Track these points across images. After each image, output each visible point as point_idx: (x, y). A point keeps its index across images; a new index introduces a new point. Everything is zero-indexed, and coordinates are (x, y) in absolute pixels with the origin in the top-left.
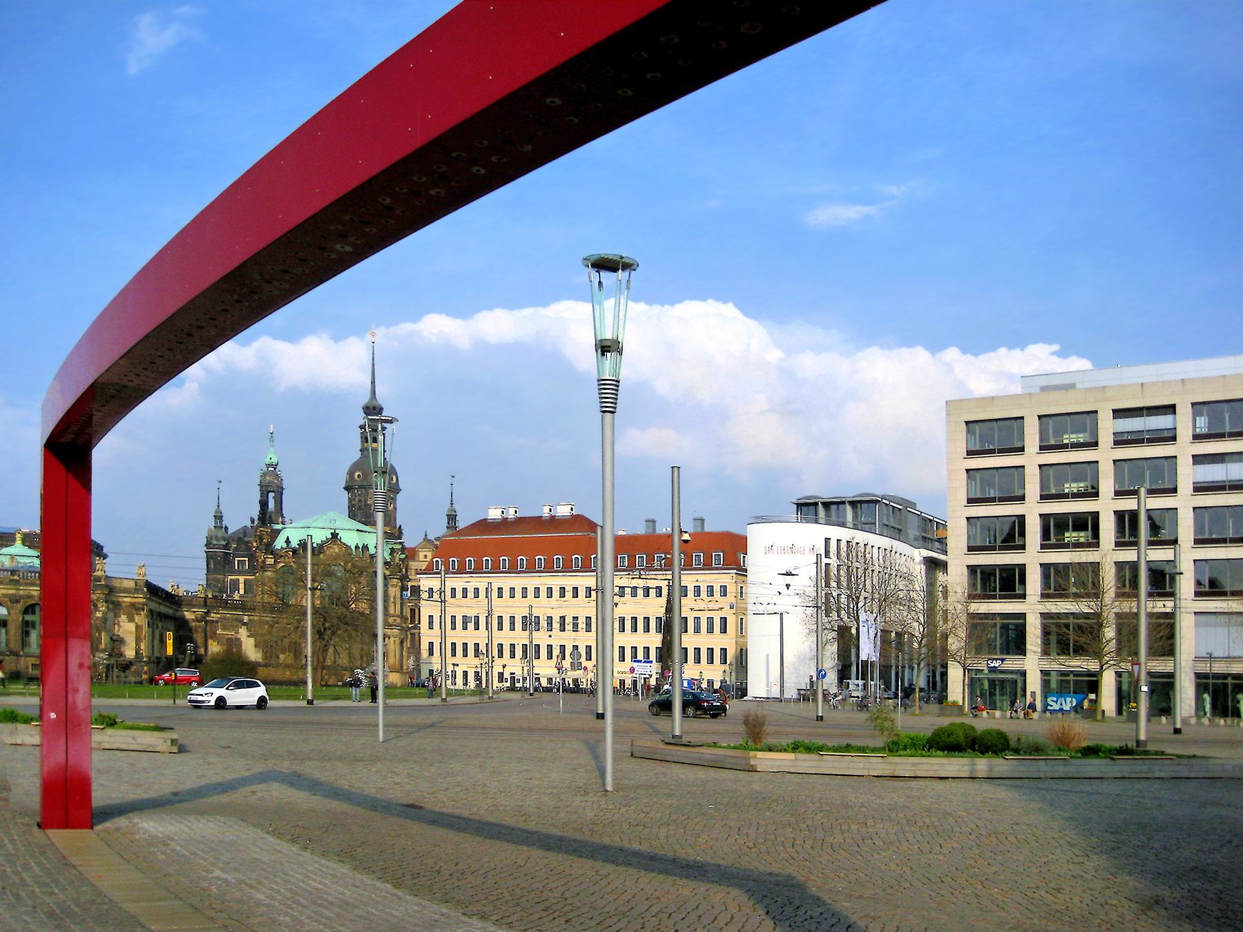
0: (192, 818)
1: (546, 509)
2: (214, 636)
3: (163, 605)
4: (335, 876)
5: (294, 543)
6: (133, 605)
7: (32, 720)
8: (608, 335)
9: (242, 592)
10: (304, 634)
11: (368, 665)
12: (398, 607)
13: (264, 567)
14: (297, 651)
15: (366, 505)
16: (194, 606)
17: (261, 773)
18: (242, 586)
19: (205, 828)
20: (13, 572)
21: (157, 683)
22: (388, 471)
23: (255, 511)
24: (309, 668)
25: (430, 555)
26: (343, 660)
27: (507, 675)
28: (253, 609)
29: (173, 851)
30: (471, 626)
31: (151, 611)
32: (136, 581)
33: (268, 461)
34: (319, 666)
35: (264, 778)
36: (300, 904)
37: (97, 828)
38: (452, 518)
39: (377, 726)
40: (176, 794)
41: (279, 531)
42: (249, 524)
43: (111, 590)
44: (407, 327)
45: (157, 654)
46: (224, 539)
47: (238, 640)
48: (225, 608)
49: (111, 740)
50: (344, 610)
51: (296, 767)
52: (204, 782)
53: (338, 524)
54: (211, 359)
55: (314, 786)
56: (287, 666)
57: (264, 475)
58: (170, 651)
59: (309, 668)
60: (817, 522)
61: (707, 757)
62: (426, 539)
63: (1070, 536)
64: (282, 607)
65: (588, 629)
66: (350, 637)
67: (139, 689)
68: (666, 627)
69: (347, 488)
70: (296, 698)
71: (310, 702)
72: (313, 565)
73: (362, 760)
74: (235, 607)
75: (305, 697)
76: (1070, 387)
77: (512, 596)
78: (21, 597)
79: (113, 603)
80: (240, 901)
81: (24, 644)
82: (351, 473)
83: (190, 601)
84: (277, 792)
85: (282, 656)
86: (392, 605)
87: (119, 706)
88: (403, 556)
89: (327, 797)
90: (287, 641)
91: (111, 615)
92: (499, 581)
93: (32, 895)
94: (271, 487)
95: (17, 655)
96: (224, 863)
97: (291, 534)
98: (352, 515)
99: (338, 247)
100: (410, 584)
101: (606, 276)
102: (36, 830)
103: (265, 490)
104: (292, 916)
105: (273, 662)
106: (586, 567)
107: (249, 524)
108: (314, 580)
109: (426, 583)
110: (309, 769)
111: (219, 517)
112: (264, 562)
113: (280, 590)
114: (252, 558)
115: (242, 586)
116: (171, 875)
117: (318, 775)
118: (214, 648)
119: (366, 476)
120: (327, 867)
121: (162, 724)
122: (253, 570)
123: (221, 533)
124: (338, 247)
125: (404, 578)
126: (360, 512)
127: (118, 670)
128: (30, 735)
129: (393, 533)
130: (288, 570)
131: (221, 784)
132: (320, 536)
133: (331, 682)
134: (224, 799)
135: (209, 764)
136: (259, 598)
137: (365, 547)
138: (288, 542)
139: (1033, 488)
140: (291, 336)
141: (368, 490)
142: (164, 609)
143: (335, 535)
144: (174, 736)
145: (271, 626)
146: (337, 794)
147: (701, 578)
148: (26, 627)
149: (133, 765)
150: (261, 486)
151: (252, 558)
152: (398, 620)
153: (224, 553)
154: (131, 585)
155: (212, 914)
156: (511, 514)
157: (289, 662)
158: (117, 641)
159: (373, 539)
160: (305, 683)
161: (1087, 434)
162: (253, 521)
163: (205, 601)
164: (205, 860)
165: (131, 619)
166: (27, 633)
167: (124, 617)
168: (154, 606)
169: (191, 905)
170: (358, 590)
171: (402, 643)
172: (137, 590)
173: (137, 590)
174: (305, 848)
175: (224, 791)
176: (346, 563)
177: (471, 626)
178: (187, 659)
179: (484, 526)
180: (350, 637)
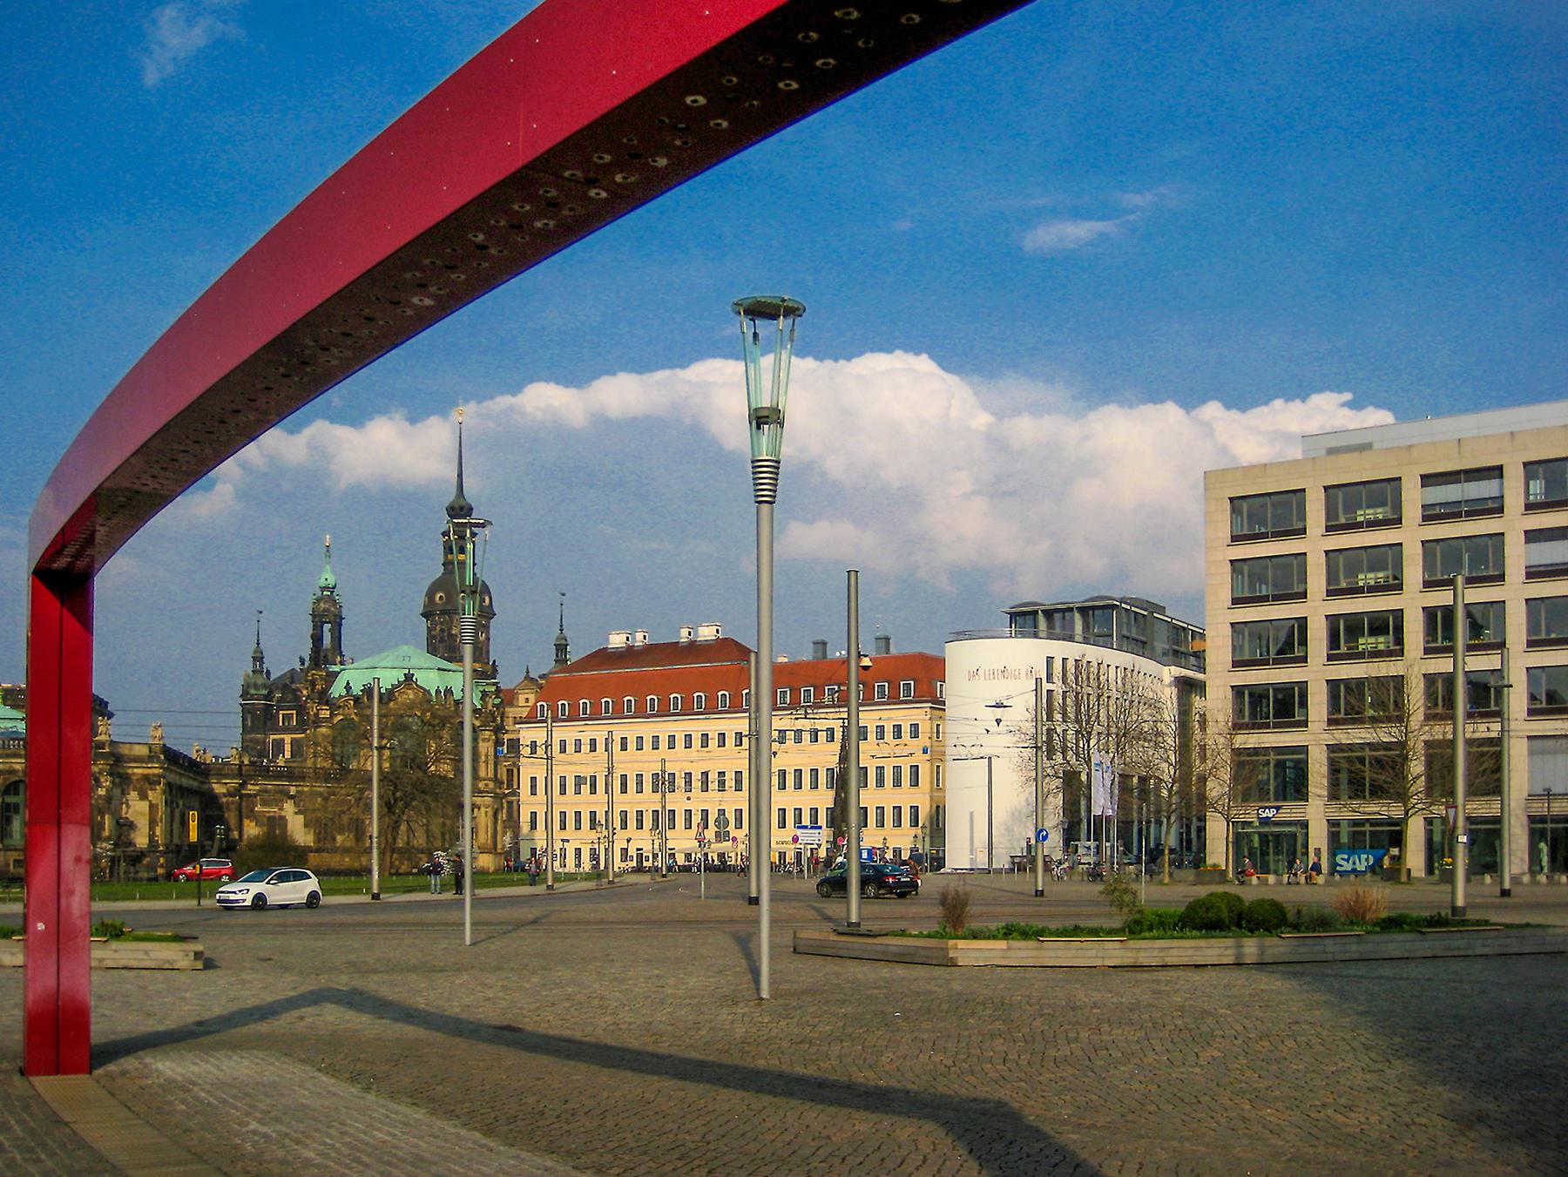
1: (684, 632)
3: (186, 779)
5: (357, 690)
6: (146, 778)
9: (288, 755)
10: (368, 807)
11: (452, 845)
13: (317, 722)
14: (359, 831)
15: (451, 635)
17: (312, 992)
18: (288, 748)
19: (237, 1067)
21: (177, 880)
23: (306, 653)
24: (375, 852)
25: (532, 698)
26: (420, 840)
27: (632, 852)
28: (302, 778)
29: (196, 1098)
30: (586, 788)
31: (169, 785)
33: (322, 583)
34: (388, 848)
37: (96, 1072)
40: (200, 1023)
41: (336, 674)
42: (298, 666)
45: (176, 841)
46: (265, 686)
47: (283, 818)
48: (265, 777)
49: (116, 956)
50: (420, 774)
51: (358, 982)
52: (236, 1006)
53: (414, 662)
55: (379, 1006)
56: (346, 851)
57: (319, 600)
58: (193, 836)
59: (375, 852)
60: (1036, 636)
61: (892, 949)
63: (1366, 578)
64: (341, 773)
66: (428, 809)
67: (155, 887)
70: (358, 891)
71: (376, 897)
72: (381, 716)
73: (442, 970)
74: (279, 775)
75: (369, 890)
76: (1367, 447)
79: (120, 776)
80: (283, 1162)
82: (430, 594)
83: (221, 771)
84: (332, 1016)
85: (339, 838)
87: (128, 912)
90: (345, 818)
91: (117, 791)
94: (327, 615)
96: (262, 1112)
97: (352, 677)
98: (432, 650)
99: (415, 300)
100: (506, 737)
102: (17, 1078)
103: (318, 619)
107: (298, 666)
108: (381, 737)
109: (527, 735)
110: (374, 984)
111: (258, 658)
112: (316, 715)
114: (301, 710)
115: (288, 748)
116: (192, 1131)
117: (386, 992)
118: (252, 830)
119: (450, 597)
121: (184, 932)
122: (302, 725)
123: (260, 680)
124: (415, 300)
125: (499, 730)
130: (347, 720)
131: (258, 1008)
133: (404, 868)
134: (264, 1027)
135: (244, 982)
136: (309, 763)
137: (449, 691)
138: (348, 687)
139: (1317, 581)
140: (356, 418)
142: (185, 782)
144: (199, 947)
145: (326, 799)
146: (408, 1015)
147: (885, 715)
151: (301, 710)
152: (491, 785)
153: (268, 703)
154: (144, 751)
156: (639, 640)
157: (348, 844)
159: (458, 680)
160: (370, 871)
161: (1388, 509)
162: (302, 661)
163: (240, 769)
164: (237, 1108)
165: (143, 796)
167: (134, 794)
170: (439, 748)
172: (150, 759)
174: (368, 1089)
175: (263, 1018)
176: (423, 713)
177: (586, 788)
178: (216, 845)
179: (604, 657)
180: (428, 809)
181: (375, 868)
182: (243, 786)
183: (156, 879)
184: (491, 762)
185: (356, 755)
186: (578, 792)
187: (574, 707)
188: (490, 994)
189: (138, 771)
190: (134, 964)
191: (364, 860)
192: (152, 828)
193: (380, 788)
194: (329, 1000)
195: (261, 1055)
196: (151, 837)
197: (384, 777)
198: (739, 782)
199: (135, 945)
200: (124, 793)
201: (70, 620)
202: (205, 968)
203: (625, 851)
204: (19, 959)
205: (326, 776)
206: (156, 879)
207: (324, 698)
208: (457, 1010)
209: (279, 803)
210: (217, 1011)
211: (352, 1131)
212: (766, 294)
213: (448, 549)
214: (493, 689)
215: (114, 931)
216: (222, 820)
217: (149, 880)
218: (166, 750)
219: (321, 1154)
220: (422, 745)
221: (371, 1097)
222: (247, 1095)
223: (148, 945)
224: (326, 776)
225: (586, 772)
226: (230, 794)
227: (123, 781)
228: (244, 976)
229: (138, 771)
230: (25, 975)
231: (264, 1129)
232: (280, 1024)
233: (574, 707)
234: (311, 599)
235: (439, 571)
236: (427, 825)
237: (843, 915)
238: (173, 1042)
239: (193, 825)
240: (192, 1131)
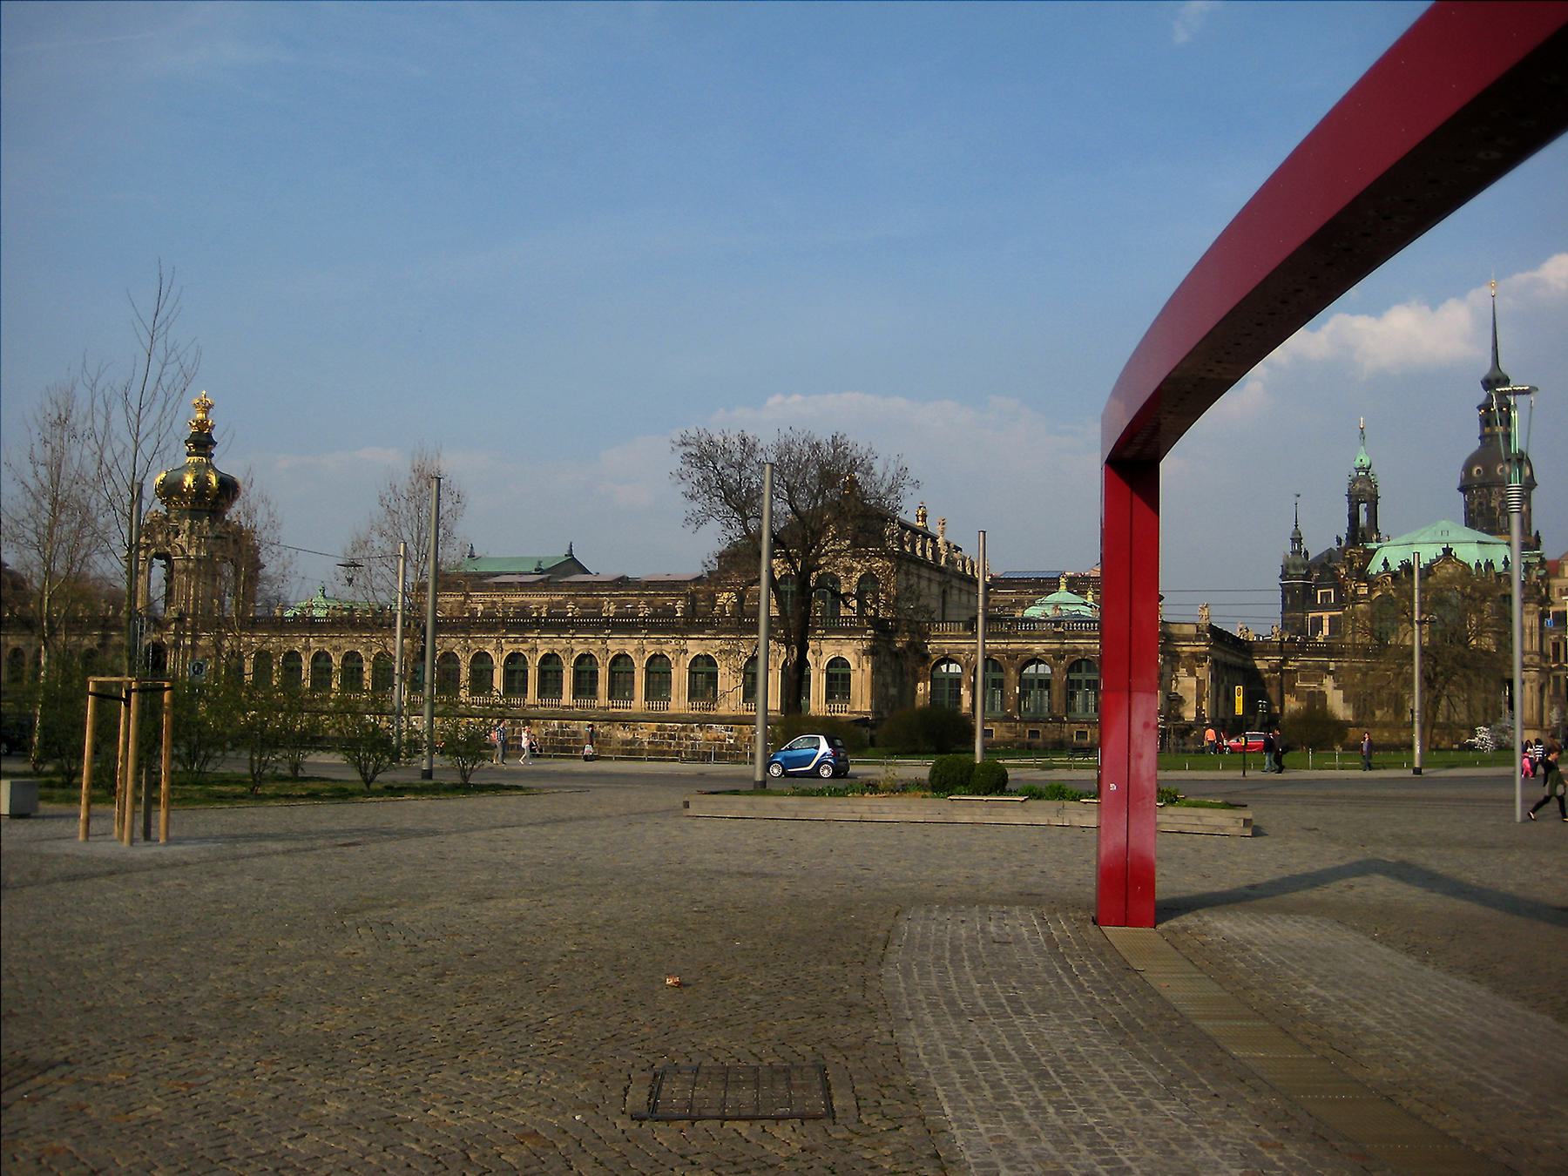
0: (1274, 917)
2: (1292, 690)
3: (1230, 654)
4: (1468, 1001)
5: (1395, 566)
6: (1193, 655)
7: (1081, 796)
9: (1326, 631)
10: (1409, 682)
11: (1495, 720)
13: (1356, 599)
14: (1399, 706)
17: (1359, 863)
18: (1326, 623)
19: (1293, 931)
20: (1058, 623)
21: (1222, 752)
23: (1343, 533)
24: (1417, 726)
26: (1461, 716)
28: (1341, 653)
29: (1255, 957)
31: (1215, 662)
33: (1357, 464)
34: (1429, 723)
35: (1365, 868)
36: (1423, 1035)
37: (1159, 927)
39: (1513, 801)
40: (1253, 887)
41: (1374, 551)
42: (1335, 546)
43: (1169, 638)
44: (1521, 278)
45: (1221, 715)
48: (1305, 654)
49: (1171, 820)
50: (1461, 649)
51: (1403, 855)
52: (1286, 873)
53: (1453, 536)
54: (1277, 354)
55: (1430, 880)
56: (1385, 726)
57: (1354, 481)
58: (1239, 710)
59: (1417, 726)
64: (1380, 647)
66: (1470, 683)
67: (1201, 758)
69: (1462, 489)
70: (1400, 766)
72: (1421, 591)
73: (1493, 846)
74: (1318, 652)
75: (1410, 764)
78: (1066, 651)
79: (1170, 653)
80: (1343, 1026)
81: (1069, 707)
82: (1468, 468)
83: (1263, 648)
84: (1380, 887)
85: (1378, 713)
86: (1527, 637)
87: (1180, 781)
88: (1542, 572)
89: (1448, 894)
90: (1384, 694)
91: (1167, 669)
93: (1091, 1003)
94: (1363, 495)
95: (1060, 720)
96: (1321, 976)
97: (1389, 554)
98: (1471, 522)
99: (1481, 155)
100: (1552, 610)
102: (1090, 926)
103: (1354, 500)
104: (1413, 1050)
105: (1367, 720)
107: (1335, 546)
108: (1421, 612)
110: (1421, 857)
111: (1297, 539)
112: (1355, 591)
113: (1376, 626)
114: (1340, 588)
115: (1326, 623)
116: (1253, 989)
117: (1434, 866)
118: (1292, 704)
119: (1488, 469)
120: (1457, 988)
121: (1233, 800)
122: (1340, 603)
123: (1300, 560)
124: (1481, 155)
125: (1545, 601)
126: (1484, 515)
127: (1177, 737)
128: (1084, 816)
129: (1531, 542)
130: (1386, 598)
131: (1306, 876)
132: (1429, 553)
133: (1444, 744)
134: (1315, 894)
135: (1291, 850)
136: (1348, 639)
137: (1490, 565)
138: (1386, 564)
140: (1376, 309)
142: (1231, 659)
143: (1447, 551)
144: (1248, 815)
145: (1365, 674)
146: (1458, 889)
148: (1071, 687)
149: (1199, 851)
150: (1350, 496)
151: (1340, 588)
152: (1537, 659)
153: (1307, 580)
154: (1192, 630)
155: (1307, 1040)
157: (1387, 719)
158: (1175, 701)
159: (1498, 553)
160: (1411, 747)
162: (1339, 541)
163: (1281, 646)
164: (1293, 970)
165: (1192, 673)
166: (1073, 696)
168: (1219, 655)
169: (1281, 1028)
170: (1481, 622)
171: (1541, 689)
172: (1198, 637)
173: (1199, 636)
174: (1425, 962)
175: (1313, 885)
176: (1464, 588)
178: (1258, 720)
180: (1470, 683)
181: (1417, 743)
182: (1284, 662)
183: (1202, 751)
185: (1395, 631)
188: (1547, 873)
189: (1186, 649)
190: (1187, 829)
191: (1404, 735)
192: (1199, 703)
193: (1421, 661)
194: (1377, 871)
195: (1314, 920)
196: (1199, 711)
197: (1424, 652)
199: (1188, 811)
200: (1174, 670)
201: (1140, 505)
202: (1254, 835)
204: (1092, 820)
205: (1365, 652)
206: (1202, 751)
207: (1362, 575)
208: (1511, 888)
210: (1268, 877)
211: (1412, 1002)
213: (1486, 421)
214: (1537, 560)
215: (1170, 798)
216: (1264, 696)
217: (1197, 751)
218: (1213, 629)
219: (1381, 1022)
220: (1463, 619)
221: (1428, 970)
222: (1304, 958)
223: (1201, 811)
224: (1365, 652)
226: (1272, 670)
227: (1174, 658)
228: (1291, 844)
229: (1186, 649)
230: (1099, 835)
231: (1322, 993)
232: (1330, 892)
234: (1348, 480)
235: (1476, 444)
236: (1468, 700)
238: (1229, 902)
239: (1239, 700)
240: (1253, 989)
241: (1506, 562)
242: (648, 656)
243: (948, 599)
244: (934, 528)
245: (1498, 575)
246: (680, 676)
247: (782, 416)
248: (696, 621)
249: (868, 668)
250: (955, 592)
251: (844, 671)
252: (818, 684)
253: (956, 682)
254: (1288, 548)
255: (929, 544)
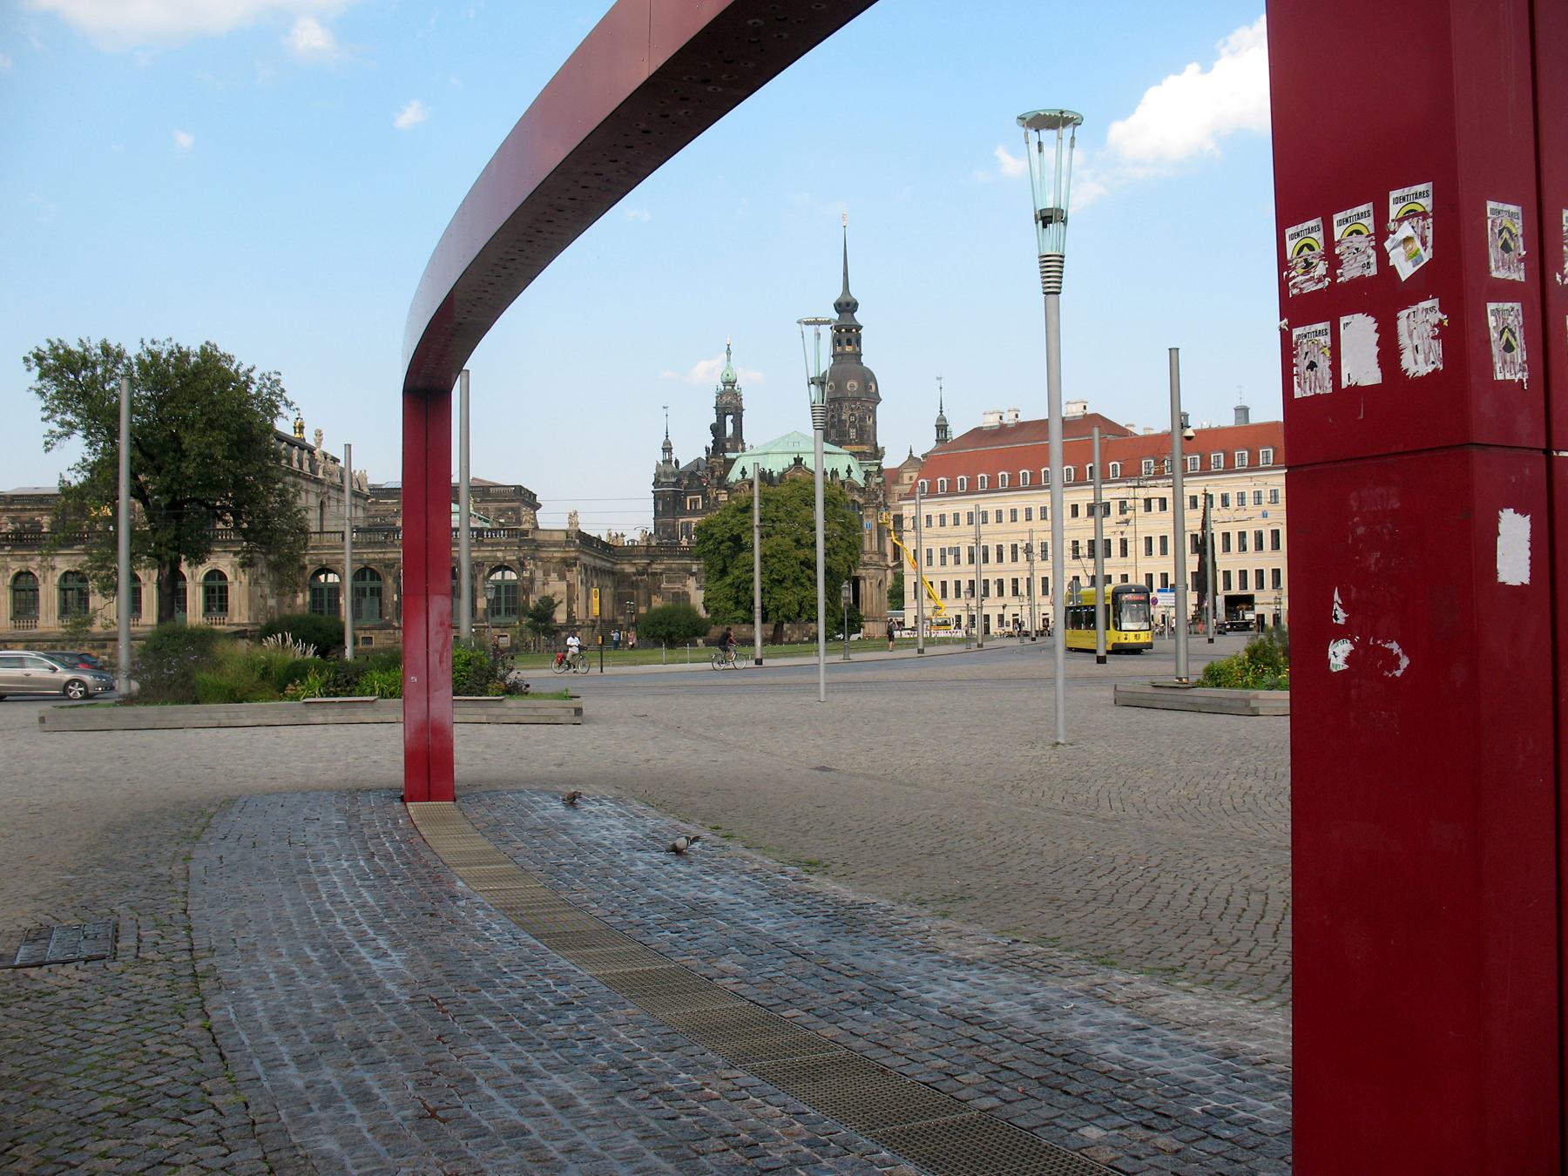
2: (658, 590)
8: (1049, 203)
12: (875, 542)
15: (840, 421)
16: (635, 556)
22: (867, 379)
23: (708, 440)
25: (915, 475)
27: (1008, 618)
32: (567, 532)
38: (942, 427)
41: (733, 461)
46: (673, 474)
47: (686, 594)
57: (720, 395)
61: (1200, 700)
62: (911, 456)
65: (1164, 551)
68: (1201, 545)
71: (759, 662)
74: (683, 555)
77: (1014, 520)
83: (629, 552)
92: (990, 504)
94: (729, 406)
101: (1048, 135)
102: (397, 804)
103: (721, 412)
106: (1036, 484)
109: (908, 510)
111: (667, 449)
123: (669, 470)
137: (835, 473)
138: (743, 472)
141: (847, 405)
142: (599, 563)
143: (798, 461)
153: (675, 489)
162: (707, 449)
165: (562, 577)
167: (554, 575)
168: (585, 559)
173: (568, 543)
177: (950, 559)
184: (875, 536)
186: (943, 563)
187: (952, 484)
198: (930, 557)
203: (1001, 617)
207: (722, 483)
209: (682, 580)
212: (1049, 104)
225: (953, 543)
233: (952, 484)
237: (1172, 670)
241: (849, 471)
242: (12, 573)
243: (326, 510)
244: (310, 440)
245: (843, 483)
246: (49, 594)
247: (146, 319)
248: (66, 538)
249: (245, 579)
250: (333, 503)
251: (222, 583)
252: (195, 598)
253: (335, 590)
254: (660, 457)
255: (306, 455)
